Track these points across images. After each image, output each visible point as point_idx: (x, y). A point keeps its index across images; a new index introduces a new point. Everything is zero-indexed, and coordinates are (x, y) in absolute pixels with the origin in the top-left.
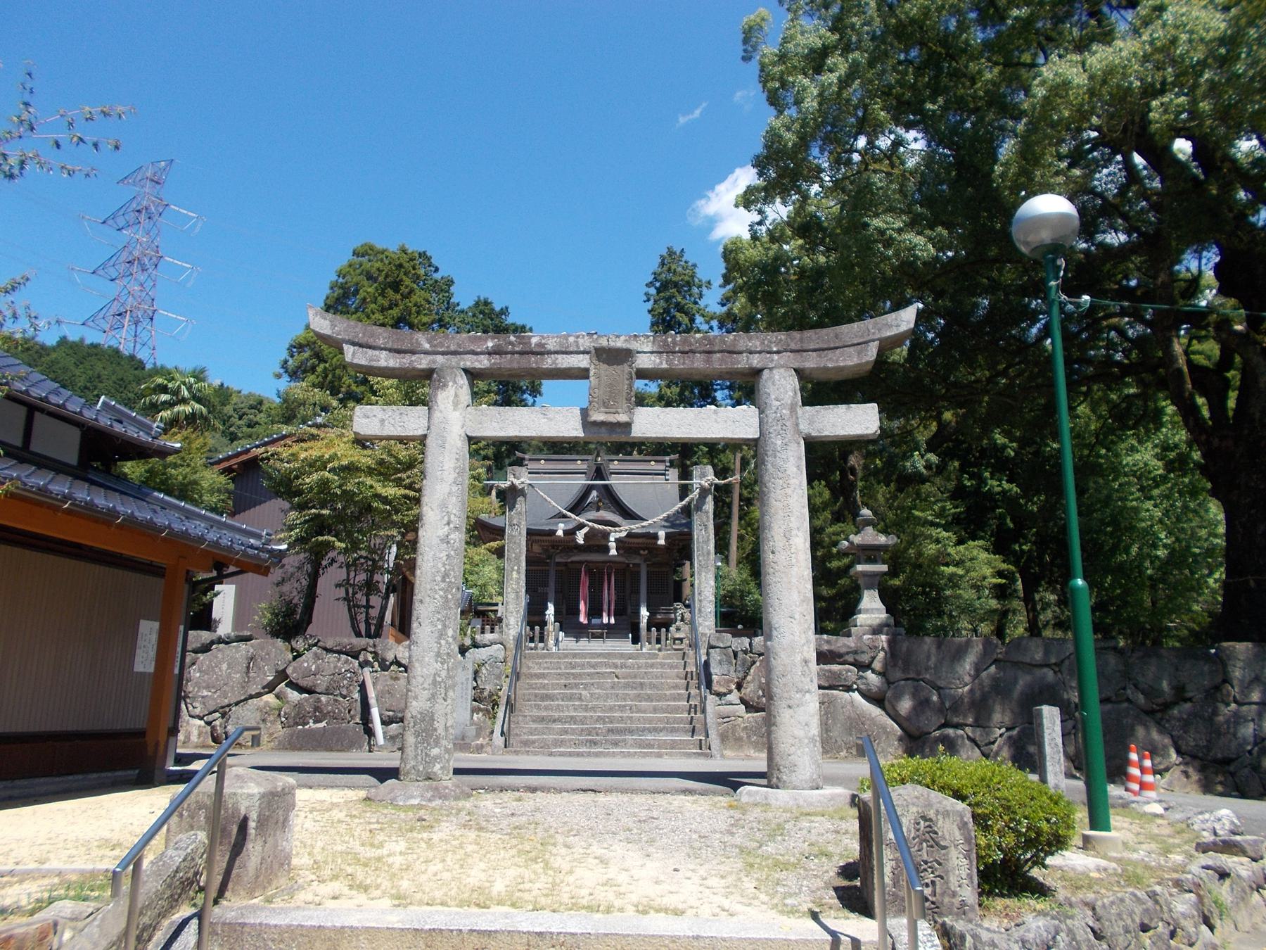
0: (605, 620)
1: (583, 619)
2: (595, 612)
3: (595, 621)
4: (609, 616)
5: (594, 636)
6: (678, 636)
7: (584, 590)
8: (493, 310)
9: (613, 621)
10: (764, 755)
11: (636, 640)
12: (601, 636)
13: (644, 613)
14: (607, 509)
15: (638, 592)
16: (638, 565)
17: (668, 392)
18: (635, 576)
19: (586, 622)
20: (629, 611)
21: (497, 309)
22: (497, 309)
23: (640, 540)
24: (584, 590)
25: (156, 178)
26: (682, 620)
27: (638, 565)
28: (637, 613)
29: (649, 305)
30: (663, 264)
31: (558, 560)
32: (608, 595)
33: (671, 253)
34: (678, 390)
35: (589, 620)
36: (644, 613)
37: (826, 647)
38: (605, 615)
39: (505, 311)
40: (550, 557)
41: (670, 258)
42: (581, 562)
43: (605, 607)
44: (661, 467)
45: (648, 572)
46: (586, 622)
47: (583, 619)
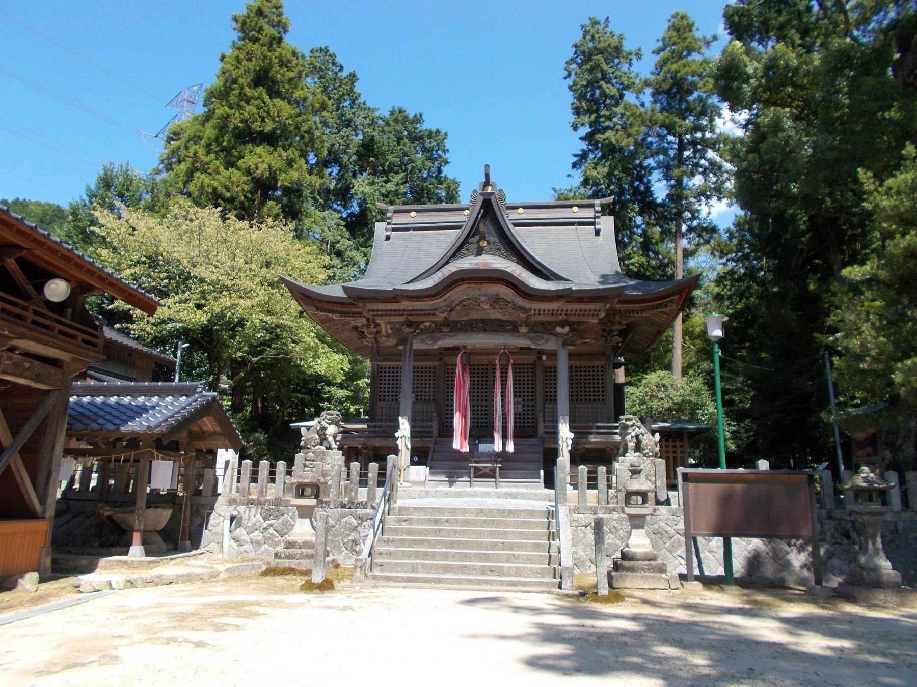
0: (498, 446)
1: (459, 444)
2: (480, 431)
3: (483, 448)
4: (504, 437)
5: (480, 474)
6: (635, 485)
7: (462, 395)
8: (406, 116)
9: (511, 448)
10: (634, 497)
11: (549, 482)
12: (491, 475)
13: (565, 434)
14: (495, 252)
15: (552, 398)
16: (552, 355)
17: (594, 173)
18: (551, 374)
19: (466, 449)
20: (541, 430)
21: (411, 116)
22: (411, 116)
23: (554, 306)
24: (462, 395)
25: (191, 100)
26: (638, 448)
27: (552, 355)
28: (555, 433)
29: (570, 82)
30: (586, 32)
31: (418, 345)
32: (505, 404)
33: (595, 23)
34: (606, 170)
35: (473, 446)
36: (565, 434)
37: (419, 445)
38: (497, 437)
39: (418, 119)
40: (403, 341)
41: (591, 30)
42: (455, 350)
43: (498, 424)
44: (588, 213)
45: (570, 368)
46: (466, 449)
47: (459, 444)
